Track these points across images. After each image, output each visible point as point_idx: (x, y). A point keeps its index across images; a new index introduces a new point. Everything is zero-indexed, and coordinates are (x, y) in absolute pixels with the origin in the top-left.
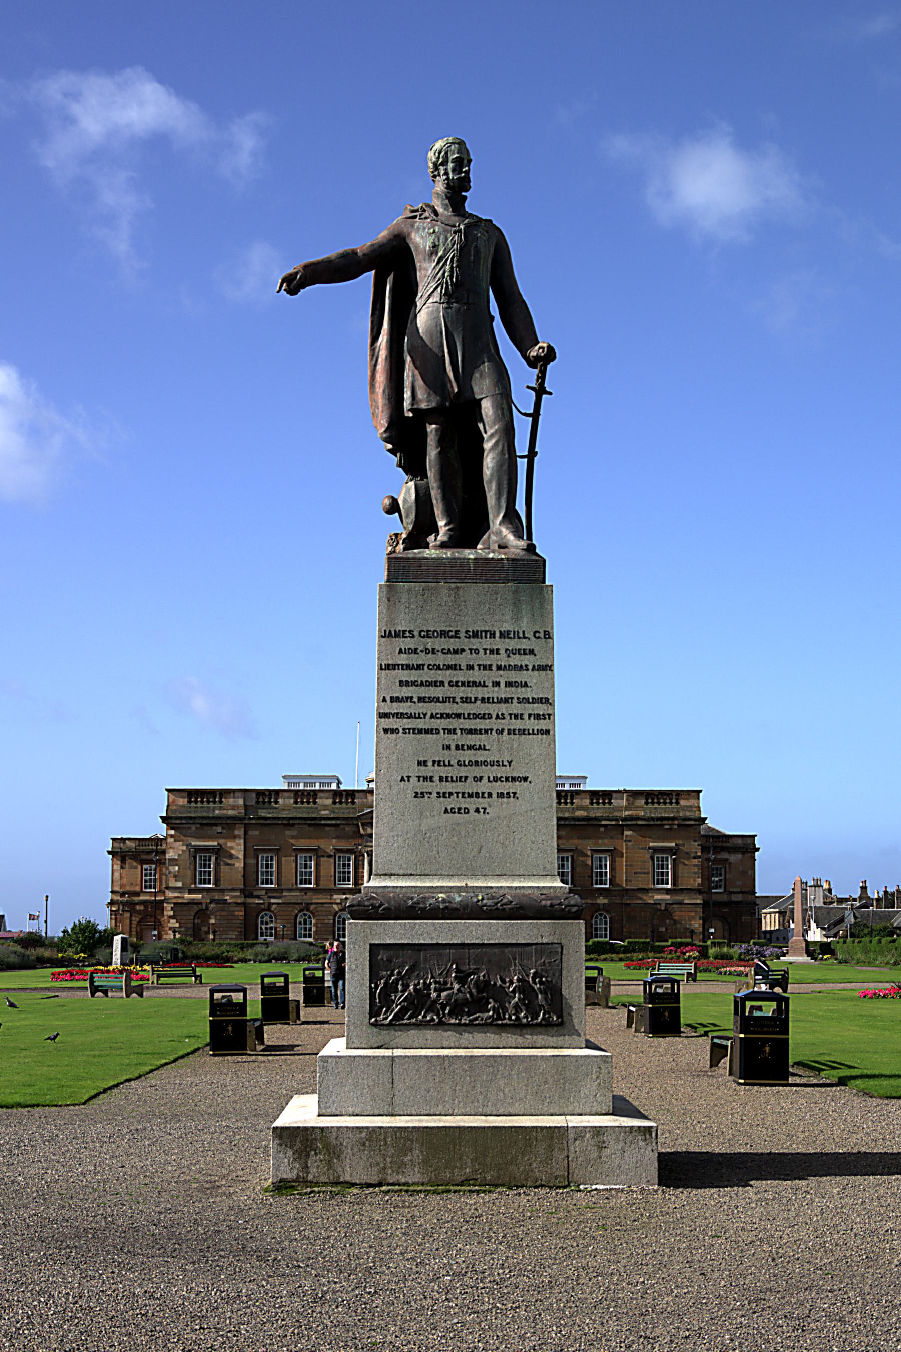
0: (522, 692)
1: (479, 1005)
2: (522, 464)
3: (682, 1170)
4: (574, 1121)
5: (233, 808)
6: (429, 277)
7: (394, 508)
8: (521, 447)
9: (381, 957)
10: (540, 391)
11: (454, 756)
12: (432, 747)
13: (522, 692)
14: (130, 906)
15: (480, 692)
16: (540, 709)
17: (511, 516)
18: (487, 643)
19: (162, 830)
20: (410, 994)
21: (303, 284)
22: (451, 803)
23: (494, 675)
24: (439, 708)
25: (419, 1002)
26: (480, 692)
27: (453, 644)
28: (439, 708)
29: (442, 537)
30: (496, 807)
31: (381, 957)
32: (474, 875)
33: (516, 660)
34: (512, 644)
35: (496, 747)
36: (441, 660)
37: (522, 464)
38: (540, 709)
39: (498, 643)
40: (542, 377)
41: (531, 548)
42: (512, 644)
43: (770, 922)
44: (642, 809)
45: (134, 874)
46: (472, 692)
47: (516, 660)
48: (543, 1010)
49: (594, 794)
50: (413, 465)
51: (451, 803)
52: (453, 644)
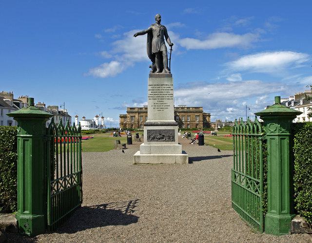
0: (169, 93)
1: (162, 138)
2: (169, 60)
3: (191, 160)
4: (177, 155)
5: (136, 110)
6: (155, 34)
7: (150, 67)
8: (169, 58)
9: (149, 131)
10: (171, 50)
11: (159, 103)
12: (156, 101)
13: (169, 93)
14: (122, 124)
15: (163, 93)
16: (172, 96)
17: (167, 67)
18: (164, 86)
19: (126, 113)
20: (154, 136)
21: (137, 35)
22: (159, 109)
23: (165, 91)
24: (157, 96)
25: (154, 138)
26: (163, 93)
27: (159, 86)
28: (157, 96)
29: (158, 71)
30: (165, 110)
31: (149, 131)
32: (162, 120)
33: (168, 89)
34: (168, 86)
35: (165, 101)
36: (157, 89)
37: (169, 60)
38: (172, 96)
39: (165, 86)
40: (171, 48)
41: (170, 73)
42: (168, 86)
43: (213, 126)
44: (194, 109)
45: (123, 119)
46: (162, 93)
47: (168, 89)
48: (171, 137)
49: (187, 108)
50: (153, 61)
51: (159, 109)
52: (159, 86)
